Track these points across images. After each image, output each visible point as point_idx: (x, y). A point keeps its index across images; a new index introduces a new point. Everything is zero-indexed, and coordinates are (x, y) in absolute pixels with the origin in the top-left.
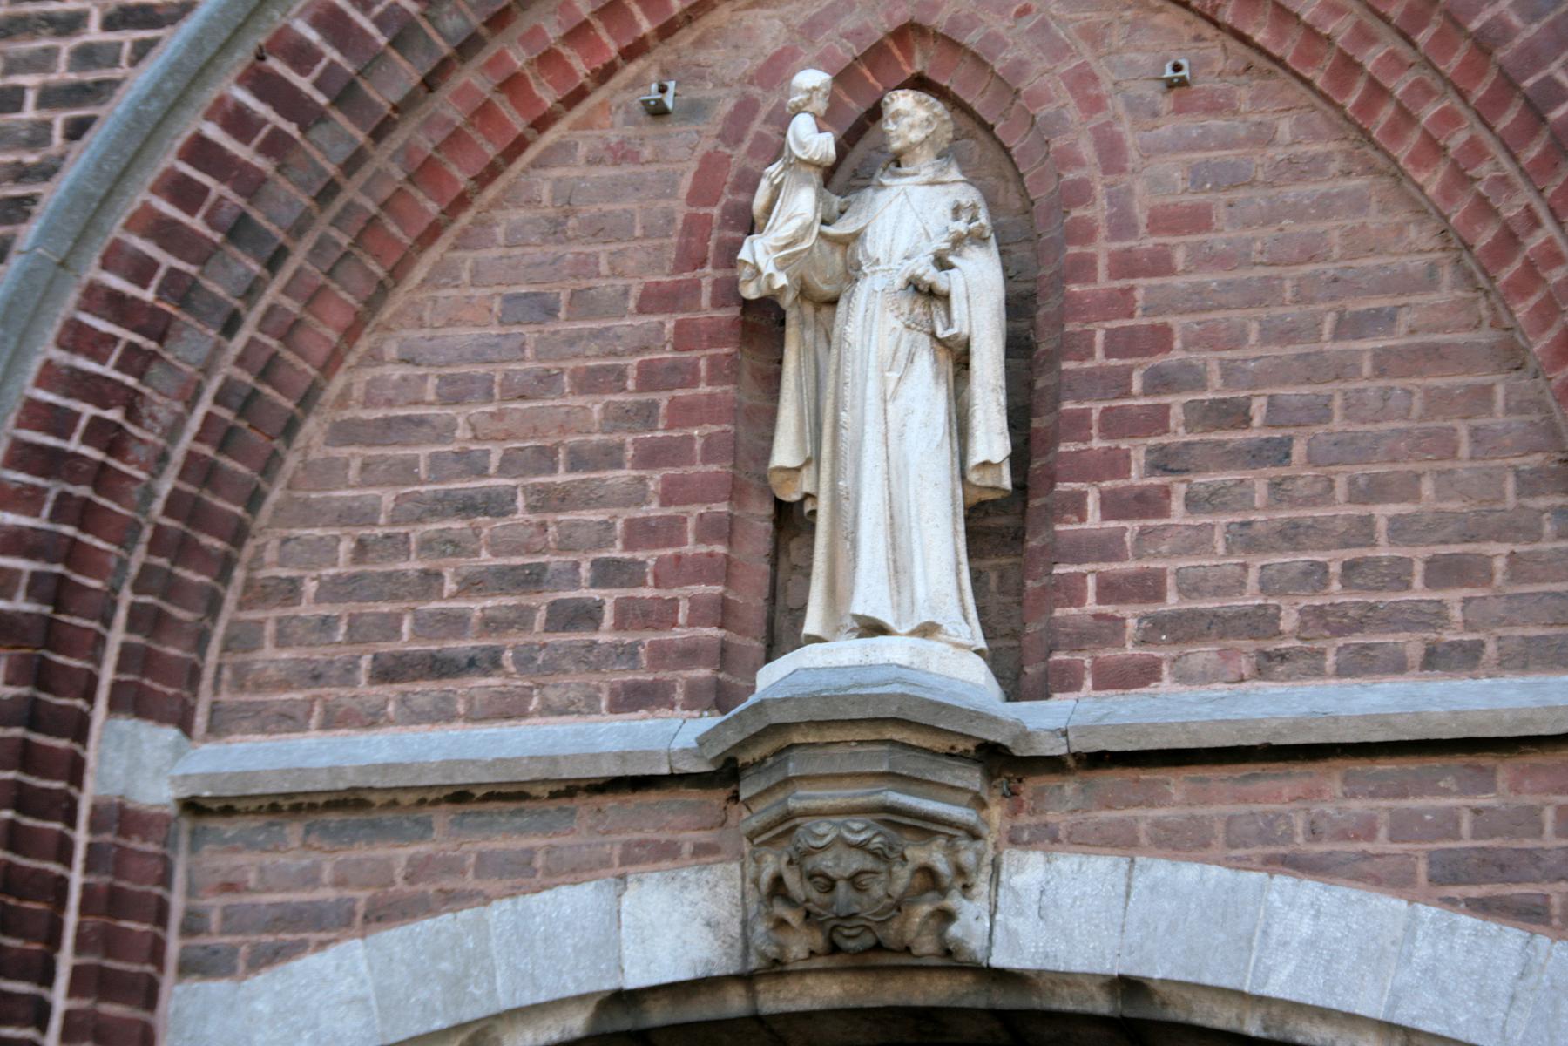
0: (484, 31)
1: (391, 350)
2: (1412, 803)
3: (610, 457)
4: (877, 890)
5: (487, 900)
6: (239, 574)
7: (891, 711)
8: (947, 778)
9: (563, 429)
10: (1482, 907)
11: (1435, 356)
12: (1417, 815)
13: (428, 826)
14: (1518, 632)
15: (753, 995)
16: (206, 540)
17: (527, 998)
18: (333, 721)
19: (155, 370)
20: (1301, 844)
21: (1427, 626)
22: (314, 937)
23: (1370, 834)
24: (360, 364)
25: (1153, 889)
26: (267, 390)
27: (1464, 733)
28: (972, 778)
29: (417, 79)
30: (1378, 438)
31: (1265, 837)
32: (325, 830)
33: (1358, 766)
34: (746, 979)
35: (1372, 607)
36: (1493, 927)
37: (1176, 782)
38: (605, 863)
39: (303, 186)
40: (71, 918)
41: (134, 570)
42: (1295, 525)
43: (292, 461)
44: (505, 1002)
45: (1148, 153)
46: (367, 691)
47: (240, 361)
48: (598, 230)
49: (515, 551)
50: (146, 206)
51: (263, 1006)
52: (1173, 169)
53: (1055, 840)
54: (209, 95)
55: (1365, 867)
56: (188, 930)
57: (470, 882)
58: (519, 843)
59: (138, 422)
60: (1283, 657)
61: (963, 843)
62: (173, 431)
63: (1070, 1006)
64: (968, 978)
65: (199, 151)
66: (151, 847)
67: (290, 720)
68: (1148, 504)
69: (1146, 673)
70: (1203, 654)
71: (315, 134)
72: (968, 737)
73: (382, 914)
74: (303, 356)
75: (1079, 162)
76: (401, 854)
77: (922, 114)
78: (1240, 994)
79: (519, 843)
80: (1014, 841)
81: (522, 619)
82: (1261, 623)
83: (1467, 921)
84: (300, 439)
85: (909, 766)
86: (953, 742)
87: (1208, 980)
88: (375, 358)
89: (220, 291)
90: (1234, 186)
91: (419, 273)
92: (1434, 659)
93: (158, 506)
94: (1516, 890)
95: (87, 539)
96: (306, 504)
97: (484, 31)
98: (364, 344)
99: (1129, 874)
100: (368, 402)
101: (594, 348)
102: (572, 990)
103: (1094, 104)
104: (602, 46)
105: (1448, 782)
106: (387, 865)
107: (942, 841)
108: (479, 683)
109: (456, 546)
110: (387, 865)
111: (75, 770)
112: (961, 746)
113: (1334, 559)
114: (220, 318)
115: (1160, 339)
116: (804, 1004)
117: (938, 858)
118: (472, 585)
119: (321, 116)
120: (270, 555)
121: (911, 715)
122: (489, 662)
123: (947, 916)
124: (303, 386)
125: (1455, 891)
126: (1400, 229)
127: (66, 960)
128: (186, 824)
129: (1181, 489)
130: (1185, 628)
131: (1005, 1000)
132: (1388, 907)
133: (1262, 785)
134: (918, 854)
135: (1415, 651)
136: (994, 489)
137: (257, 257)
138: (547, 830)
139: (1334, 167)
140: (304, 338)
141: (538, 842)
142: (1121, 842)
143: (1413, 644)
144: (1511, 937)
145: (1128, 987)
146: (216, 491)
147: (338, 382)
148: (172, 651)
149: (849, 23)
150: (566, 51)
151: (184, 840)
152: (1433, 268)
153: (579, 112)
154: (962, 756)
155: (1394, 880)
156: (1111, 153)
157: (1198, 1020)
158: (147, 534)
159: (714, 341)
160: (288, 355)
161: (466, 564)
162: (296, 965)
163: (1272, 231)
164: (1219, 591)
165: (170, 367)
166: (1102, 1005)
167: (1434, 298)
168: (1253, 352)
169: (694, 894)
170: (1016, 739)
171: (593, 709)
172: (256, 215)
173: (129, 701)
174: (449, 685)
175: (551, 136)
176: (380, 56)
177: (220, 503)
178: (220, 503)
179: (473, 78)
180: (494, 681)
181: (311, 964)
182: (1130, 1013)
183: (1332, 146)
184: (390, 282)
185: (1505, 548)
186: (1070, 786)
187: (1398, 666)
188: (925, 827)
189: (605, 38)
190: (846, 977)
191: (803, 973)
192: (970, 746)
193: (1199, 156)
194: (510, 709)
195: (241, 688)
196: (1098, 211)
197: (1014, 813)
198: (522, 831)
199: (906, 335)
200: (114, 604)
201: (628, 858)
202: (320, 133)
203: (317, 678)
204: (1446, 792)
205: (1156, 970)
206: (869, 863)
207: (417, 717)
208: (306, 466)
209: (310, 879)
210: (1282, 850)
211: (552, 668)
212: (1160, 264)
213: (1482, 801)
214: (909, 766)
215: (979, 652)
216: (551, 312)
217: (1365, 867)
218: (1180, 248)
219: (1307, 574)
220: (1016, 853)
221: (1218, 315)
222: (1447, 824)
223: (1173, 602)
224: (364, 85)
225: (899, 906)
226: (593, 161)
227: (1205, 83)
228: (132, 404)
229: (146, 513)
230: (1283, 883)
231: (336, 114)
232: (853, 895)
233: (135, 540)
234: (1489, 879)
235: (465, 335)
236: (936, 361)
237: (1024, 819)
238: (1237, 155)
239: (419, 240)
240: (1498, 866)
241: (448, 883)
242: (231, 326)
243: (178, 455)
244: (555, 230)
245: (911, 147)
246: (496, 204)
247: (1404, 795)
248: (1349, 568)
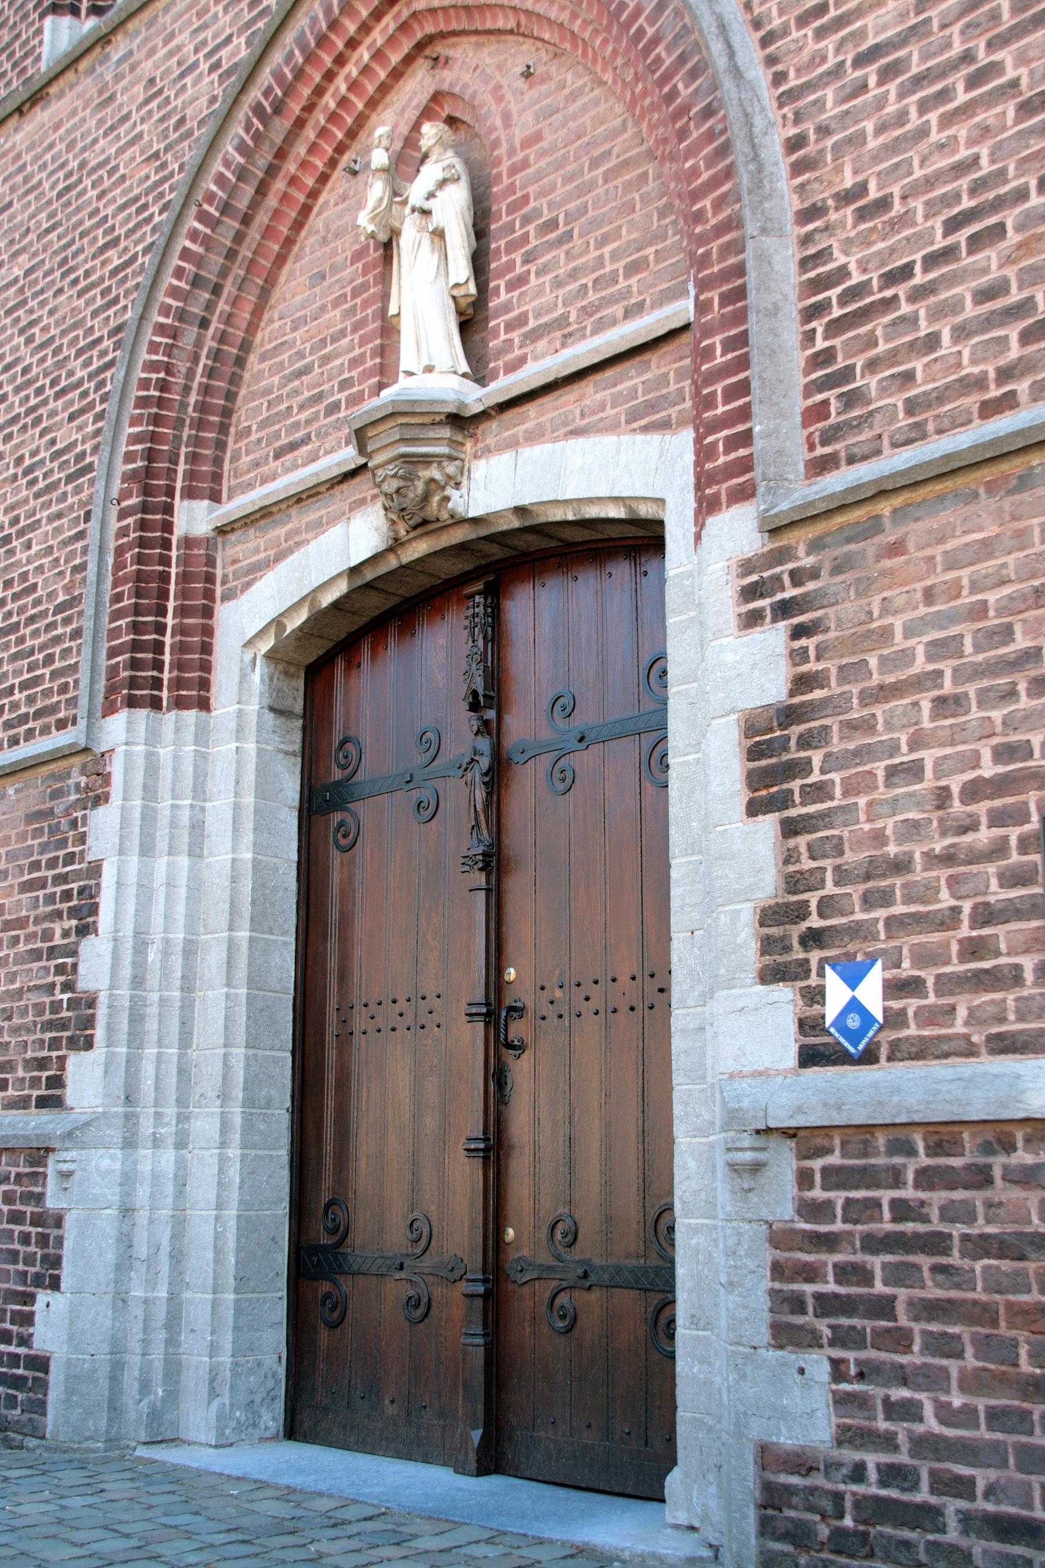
0: (275, 162)
1: (276, 316)
2: (619, 388)
3: (343, 333)
4: (411, 495)
5: (308, 541)
6: (232, 430)
7: (390, 410)
8: (432, 435)
9: (328, 328)
10: (645, 429)
11: (625, 164)
12: (620, 393)
13: (290, 516)
14: (658, 289)
15: (398, 557)
16: (212, 418)
17: (321, 581)
18: (264, 481)
19: (175, 351)
20: (580, 423)
21: (624, 298)
22: (259, 574)
23: (603, 408)
24: (267, 325)
25: (525, 463)
26: (225, 347)
27: (628, 346)
28: (446, 432)
29: (253, 192)
30: (604, 214)
31: (565, 424)
32: (261, 529)
33: (598, 377)
34: (391, 549)
35: (603, 298)
36: (649, 437)
37: (531, 409)
38: (344, 514)
39: (219, 254)
40: (172, 587)
41: (185, 438)
42: (575, 269)
43: (247, 376)
44: (315, 585)
45: (521, 113)
46: (273, 464)
47: (213, 338)
48: (337, 236)
49: (314, 388)
50: (170, 284)
51: (245, 608)
52: (529, 117)
53: (490, 452)
54: (185, 230)
55: (601, 425)
56: (223, 583)
57: (304, 536)
58: (318, 514)
59: (173, 376)
60: (570, 335)
61: (445, 464)
62: (190, 374)
63: (505, 528)
64: (467, 526)
65: (186, 255)
66: (202, 552)
67: (250, 486)
68: (522, 280)
69: (522, 361)
70: (542, 344)
71: (218, 230)
72: (439, 413)
73: (279, 557)
74: (238, 329)
75: (496, 129)
76: (281, 531)
77: (434, 131)
78: (556, 502)
79: (318, 514)
80: (475, 457)
81: (316, 417)
82: (562, 321)
83: (639, 437)
84: (249, 365)
85: (410, 434)
86: (432, 417)
87: (545, 499)
88: (271, 321)
89: (196, 310)
90: (551, 115)
91: (282, 278)
92: (628, 314)
93: (190, 409)
94: (658, 416)
95: (160, 430)
96: (252, 392)
97: (275, 162)
98: (266, 317)
99: (516, 459)
100: (270, 341)
101: (337, 287)
102: (335, 573)
103: (500, 99)
104: (325, 151)
105: (633, 373)
106: (278, 537)
107: (435, 465)
108: (305, 449)
109: (296, 392)
110: (278, 537)
111: (168, 527)
112: (438, 418)
113: (588, 280)
114: (197, 322)
115: (525, 199)
116: (416, 556)
117: (434, 473)
118: (302, 407)
119: (219, 222)
120: (243, 419)
121: (401, 409)
122: (306, 440)
123: (447, 499)
124: (239, 342)
125: (635, 425)
126: (611, 108)
127: (171, 605)
128: (220, 539)
129: (533, 269)
130: (533, 336)
131: (483, 532)
132: (608, 441)
133: (563, 399)
134: (425, 474)
135: (620, 313)
136: (467, 296)
137: (207, 291)
138: (327, 506)
139: (587, 89)
140: (236, 321)
141: (323, 512)
142: (513, 444)
143: (618, 310)
144: (655, 439)
145: (520, 511)
146: (212, 397)
147: (259, 336)
148: (204, 468)
149: (415, 102)
150: (311, 159)
151: (220, 546)
152: (624, 121)
153: (329, 185)
154: (440, 423)
155: (612, 427)
156: (507, 118)
157: (551, 519)
158: (188, 421)
159: (375, 267)
160: (231, 330)
161: (300, 399)
162: (253, 588)
163: (565, 130)
164: (549, 311)
165: (181, 348)
166: (515, 523)
167: (626, 136)
168: (557, 195)
169: (372, 518)
170: (458, 408)
171: (340, 448)
172: (202, 273)
173: (190, 493)
174: (296, 453)
175: (321, 200)
176: (235, 187)
177: (215, 401)
178: (215, 401)
179: (279, 185)
180: (309, 447)
181: (258, 585)
182: (527, 524)
183: (587, 78)
184: (268, 286)
185: (652, 249)
186: (494, 425)
187: (614, 323)
188: (426, 460)
189: (326, 147)
190: (426, 538)
191: (410, 541)
192: (443, 417)
193: (538, 106)
194: (314, 458)
195: (236, 477)
196: (502, 151)
197: (475, 444)
198: (318, 509)
199: (419, 236)
200: (178, 455)
201: (351, 510)
202: (221, 229)
203: (258, 465)
204: (632, 378)
205: (525, 501)
206: (401, 483)
207: (287, 470)
208: (253, 376)
209: (257, 551)
210: (572, 427)
211: (327, 434)
212: (525, 164)
213: (645, 377)
214: (410, 434)
215: (464, 375)
216: (324, 278)
217: (601, 425)
218: (531, 153)
219: (579, 291)
220: (476, 462)
221: (545, 180)
222: (633, 393)
223: (532, 324)
224: (233, 202)
225: (426, 498)
226: (336, 204)
227: (539, 70)
228: (169, 369)
229: (186, 413)
230: (572, 442)
231: (225, 219)
232: (401, 499)
233: (183, 426)
234: (648, 415)
235: (298, 299)
236: (432, 242)
237: (480, 445)
238: (1027, 147)
239: (274, 263)
240: (652, 407)
241: (296, 539)
242: (204, 324)
243: (195, 385)
244: (324, 241)
245: (430, 148)
246: (306, 238)
247: (615, 385)
248: (596, 281)
